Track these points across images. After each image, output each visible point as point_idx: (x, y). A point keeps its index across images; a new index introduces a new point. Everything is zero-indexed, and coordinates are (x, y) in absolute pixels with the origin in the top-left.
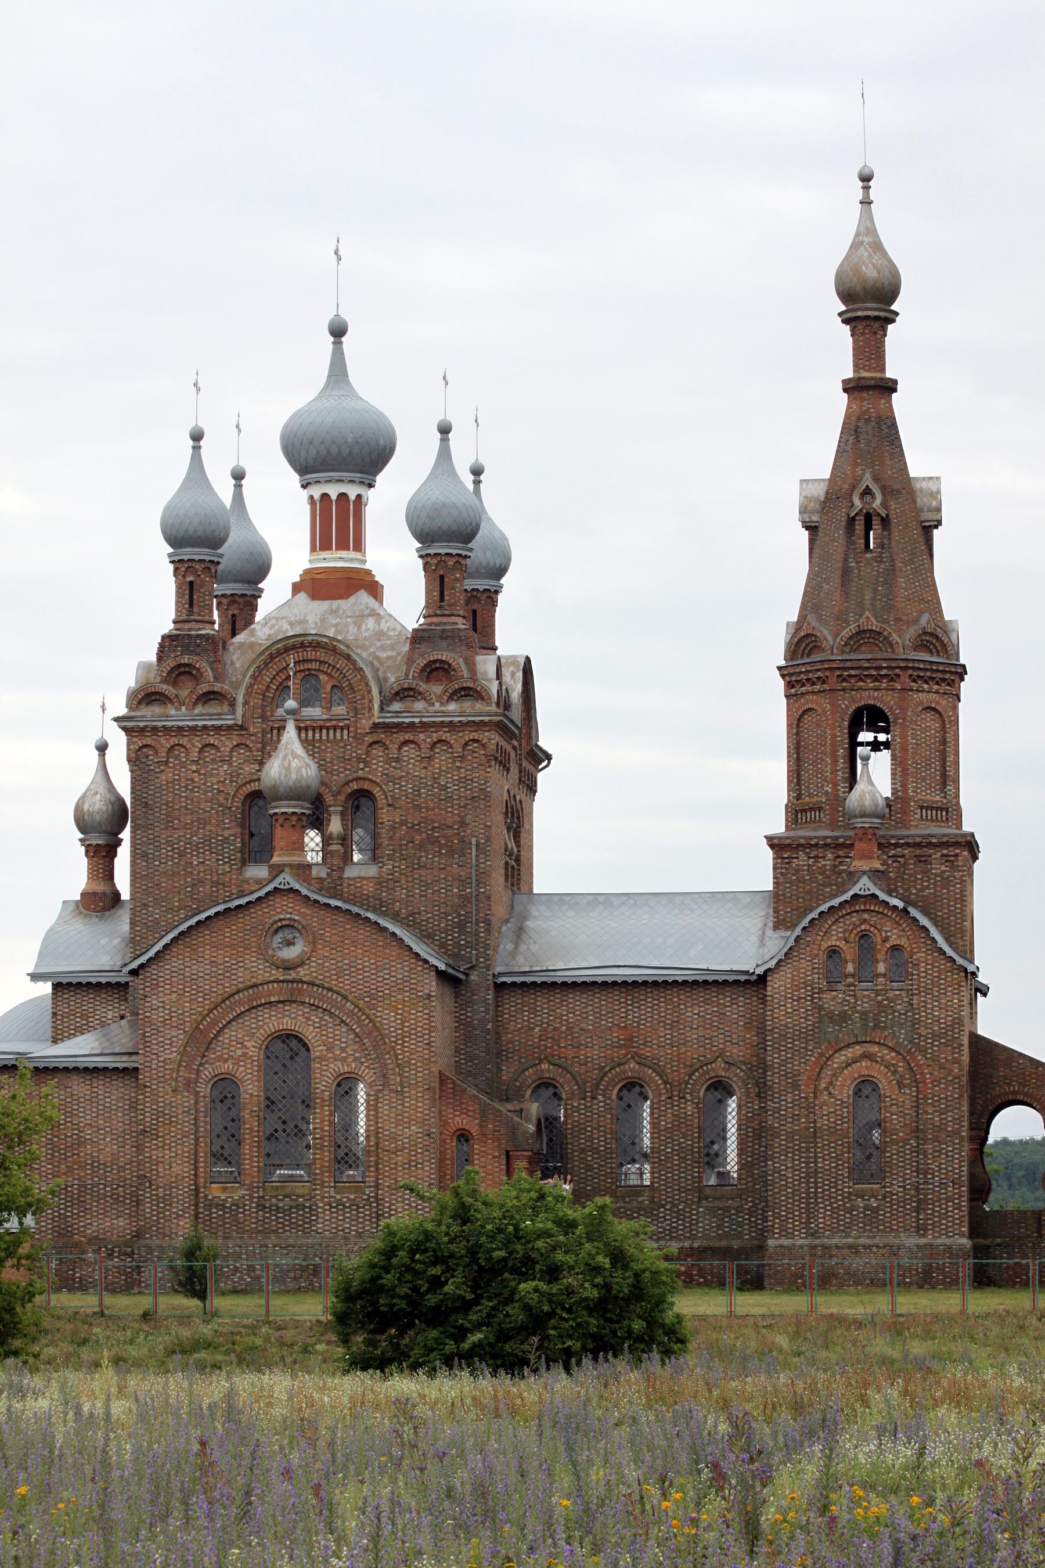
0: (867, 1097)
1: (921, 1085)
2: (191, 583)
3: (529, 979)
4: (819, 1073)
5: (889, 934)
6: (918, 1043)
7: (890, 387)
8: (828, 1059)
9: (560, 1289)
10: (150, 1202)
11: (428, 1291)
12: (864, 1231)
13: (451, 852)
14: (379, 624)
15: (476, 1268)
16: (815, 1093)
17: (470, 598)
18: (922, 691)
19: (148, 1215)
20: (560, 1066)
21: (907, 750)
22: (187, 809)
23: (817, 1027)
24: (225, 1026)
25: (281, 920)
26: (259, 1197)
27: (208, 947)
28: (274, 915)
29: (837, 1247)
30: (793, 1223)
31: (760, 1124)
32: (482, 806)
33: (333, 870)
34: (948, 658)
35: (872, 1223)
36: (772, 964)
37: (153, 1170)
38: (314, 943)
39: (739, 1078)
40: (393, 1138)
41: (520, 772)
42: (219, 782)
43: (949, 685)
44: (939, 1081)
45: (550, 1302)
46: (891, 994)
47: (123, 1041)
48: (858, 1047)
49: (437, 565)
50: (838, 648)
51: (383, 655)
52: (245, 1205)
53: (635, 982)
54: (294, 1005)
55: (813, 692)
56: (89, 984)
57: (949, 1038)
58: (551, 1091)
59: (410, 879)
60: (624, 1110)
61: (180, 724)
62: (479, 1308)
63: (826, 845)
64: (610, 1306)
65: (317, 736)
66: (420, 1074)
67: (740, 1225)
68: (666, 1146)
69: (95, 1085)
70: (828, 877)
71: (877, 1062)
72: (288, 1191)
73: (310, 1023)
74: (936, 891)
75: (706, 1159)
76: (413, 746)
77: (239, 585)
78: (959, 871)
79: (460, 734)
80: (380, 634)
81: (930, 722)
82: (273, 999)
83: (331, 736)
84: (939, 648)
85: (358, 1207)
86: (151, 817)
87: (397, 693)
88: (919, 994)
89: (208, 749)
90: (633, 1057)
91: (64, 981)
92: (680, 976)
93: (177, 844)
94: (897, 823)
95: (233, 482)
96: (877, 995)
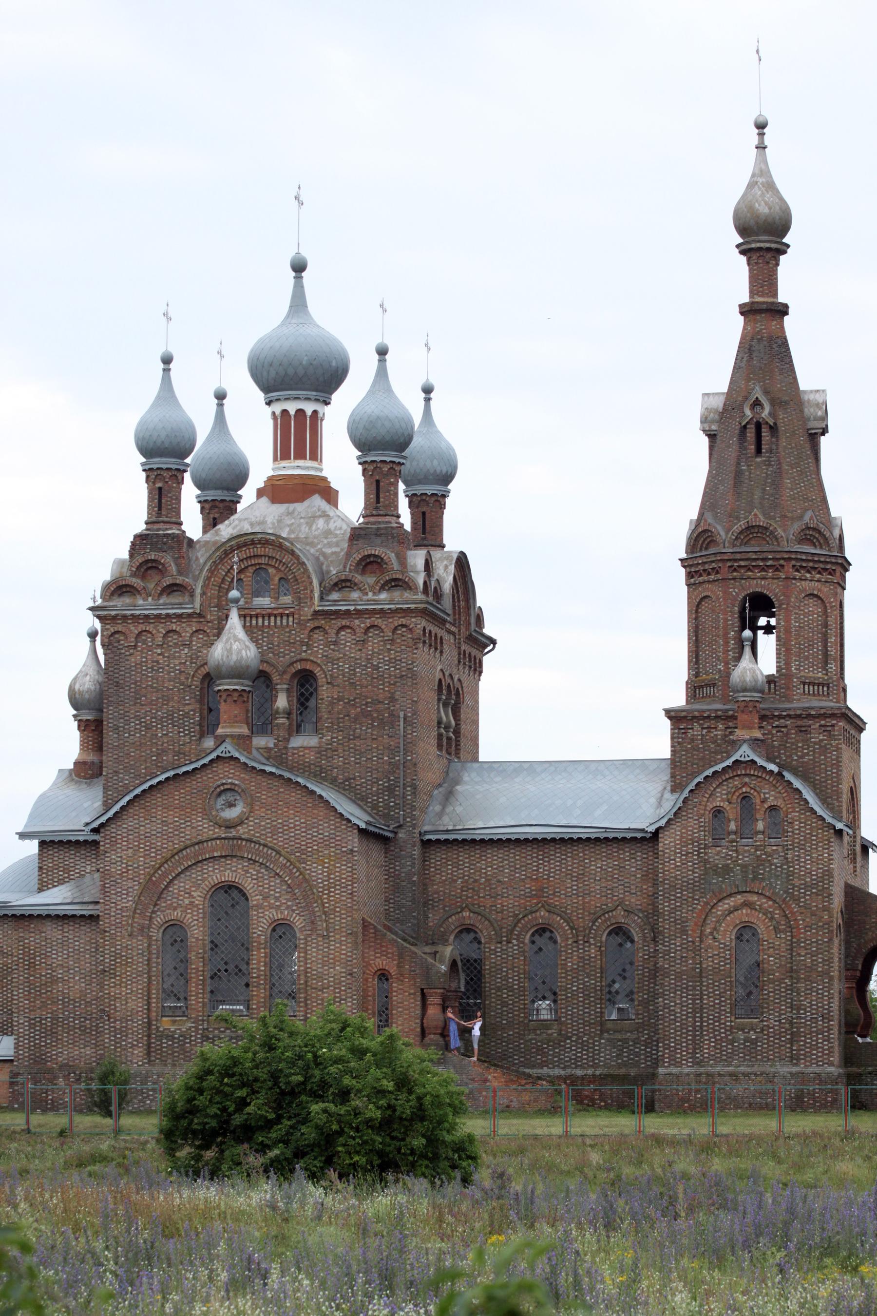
0: (748, 941)
1: (794, 930)
2: (160, 489)
3: (451, 837)
4: (705, 920)
5: (767, 796)
6: (793, 893)
7: (782, 311)
8: (712, 907)
9: (347, 1111)
10: (109, 1034)
11: (235, 1112)
12: (744, 1061)
13: (382, 723)
14: (328, 525)
15: (278, 1090)
16: (700, 937)
17: (420, 502)
18: (806, 580)
19: (107, 1045)
20: (479, 914)
21: (791, 632)
23: (703, 879)
24: (174, 878)
25: (223, 784)
26: (204, 1029)
27: (160, 808)
28: (217, 780)
29: (720, 1075)
30: (681, 1053)
31: (655, 965)
32: (409, 684)
33: (279, 741)
34: (829, 550)
35: (751, 1053)
36: (662, 823)
37: (111, 1005)
38: (252, 805)
39: (637, 924)
40: (320, 978)
41: (459, 654)
42: (181, 663)
43: (830, 574)
44: (810, 927)
45: (339, 1122)
46: (768, 849)
47: (92, 892)
48: (739, 897)
49: (373, 471)
50: (729, 542)
51: (328, 551)
52: (191, 1036)
53: (544, 839)
54: (235, 860)
55: (709, 582)
56: (69, 842)
57: (820, 888)
58: (472, 935)
59: (347, 748)
60: (536, 952)
61: (147, 612)
62: (279, 1126)
63: (717, 717)
64: (395, 1126)
65: (266, 623)
66: (344, 921)
67: (637, 1055)
68: (572, 984)
69: (66, 930)
70: (719, 745)
71: (756, 909)
73: (249, 875)
74: (815, 757)
75: (608, 996)
76: (349, 631)
77: (219, 492)
78: (835, 740)
79: (390, 620)
80: (328, 533)
81: (812, 606)
82: (216, 854)
83: (279, 622)
84: (822, 541)
86: (122, 695)
87: (336, 584)
88: (793, 849)
89: (171, 635)
90: (543, 906)
91: (48, 839)
92: (583, 834)
93: (144, 718)
94: (781, 697)
95: (216, 401)
96: (756, 850)
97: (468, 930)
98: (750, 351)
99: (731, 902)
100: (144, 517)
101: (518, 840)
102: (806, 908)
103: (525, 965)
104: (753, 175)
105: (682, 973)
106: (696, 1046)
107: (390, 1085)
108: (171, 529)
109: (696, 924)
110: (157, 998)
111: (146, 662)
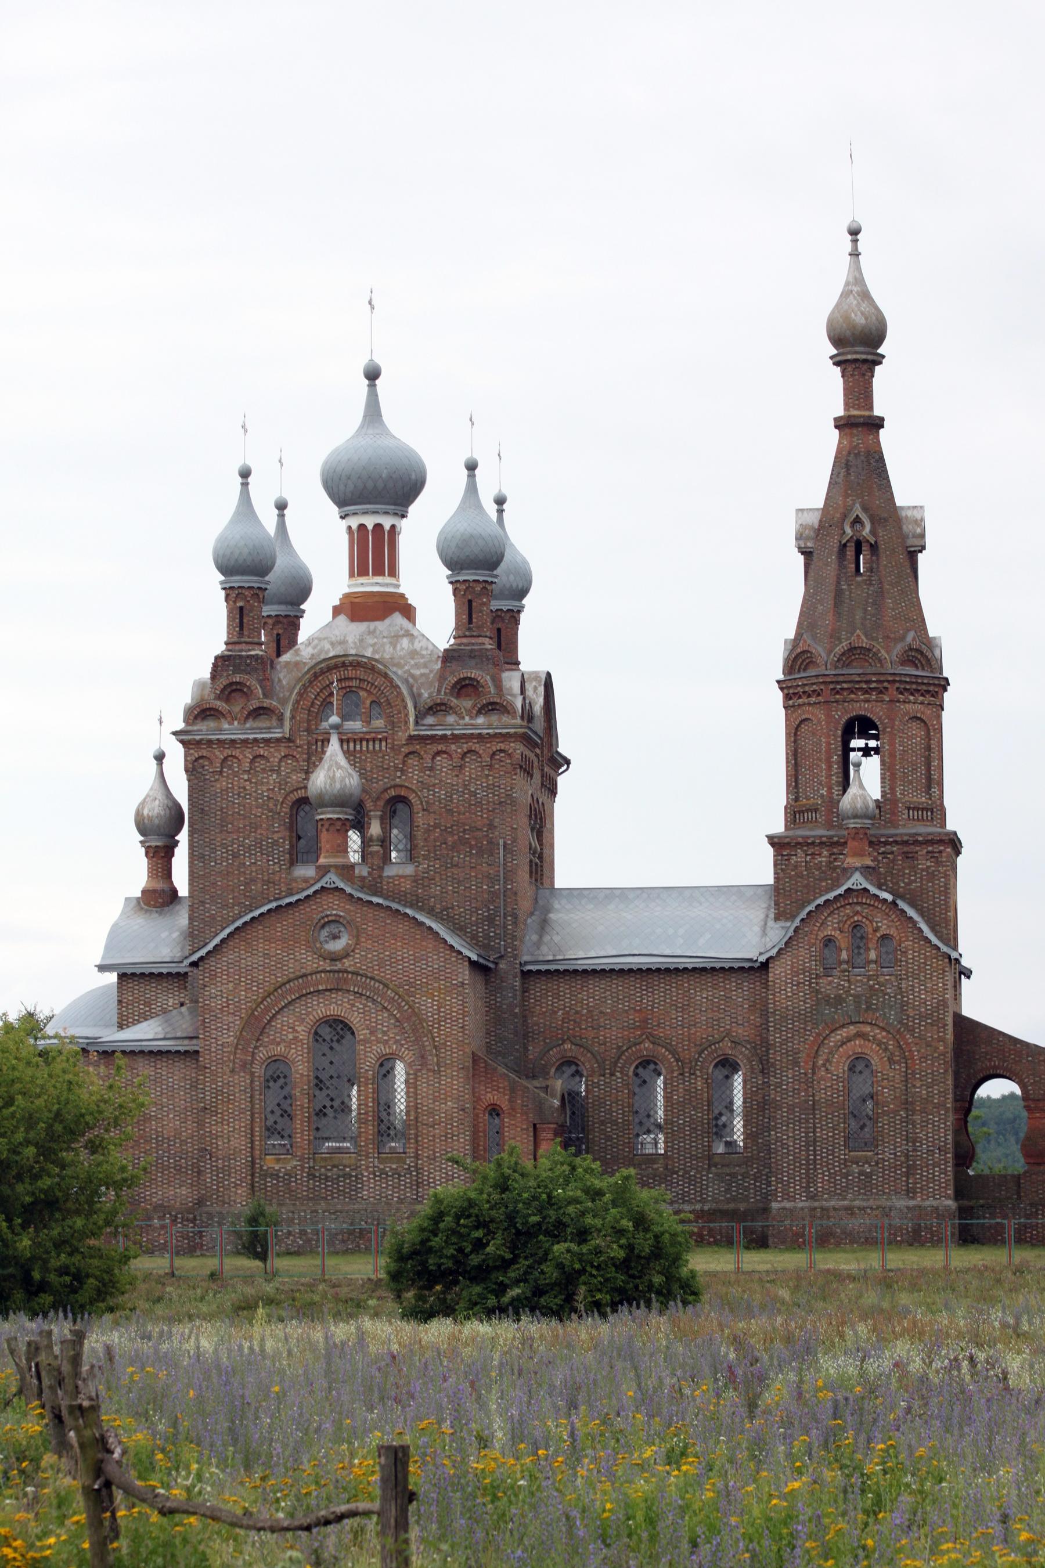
2: (241, 608)
3: (552, 967)
4: (817, 1051)
7: (878, 424)
8: (825, 1039)
11: (471, 1252)
13: (481, 852)
16: (813, 1069)
18: (909, 702)
22: (240, 815)
24: (277, 1013)
25: (327, 916)
28: (327, 910)
29: (835, 1209)
33: (373, 870)
34: (932, 672)
39: (744, 1055)
40: (431, 1113)
42: (269, 790)
43: (933, 696)
44: (925, 1058)
45: (580, 1261)
46: (881, 979)
48: (852, 1027)
49: (465, 591)
55: (809, 704)
58: (573, 1068)
61: (233, 737)
62: (517, 1266)
63: (822, 843)
64: (633, 1264)
65: (358, 747)
67: (747, 1189)
69: (159, 1066)
72: (336, 1162)
75: (714, 1130)
77: (283, 607)
80: (413, 653)
81: (916, 731)
82: (320, 988)
83: (371, 747)
85: (400, 1176)
87: (431, 708)
89: (258, 760)
90: (647, 1038)
91: (129, 971)
95: (277, 512)
96: (869, 980)
97: (569, 1062)
98: (848, 466)
99: (844, 1033)
100: (224, 637)
101: (622, 971)
102: (921, 1039)
103: (629, 1098)
104: (847, 284)
105: (794, 1106)
106: (810, 1180)
107: (627, 1224)
108: (253, 650)
109: (808, 1055)
110: (260, 1136)
111: (232, 788)
